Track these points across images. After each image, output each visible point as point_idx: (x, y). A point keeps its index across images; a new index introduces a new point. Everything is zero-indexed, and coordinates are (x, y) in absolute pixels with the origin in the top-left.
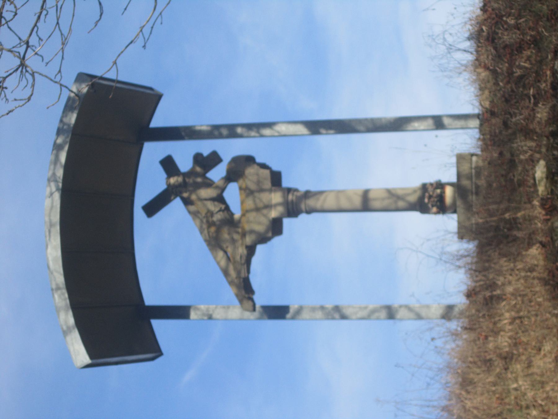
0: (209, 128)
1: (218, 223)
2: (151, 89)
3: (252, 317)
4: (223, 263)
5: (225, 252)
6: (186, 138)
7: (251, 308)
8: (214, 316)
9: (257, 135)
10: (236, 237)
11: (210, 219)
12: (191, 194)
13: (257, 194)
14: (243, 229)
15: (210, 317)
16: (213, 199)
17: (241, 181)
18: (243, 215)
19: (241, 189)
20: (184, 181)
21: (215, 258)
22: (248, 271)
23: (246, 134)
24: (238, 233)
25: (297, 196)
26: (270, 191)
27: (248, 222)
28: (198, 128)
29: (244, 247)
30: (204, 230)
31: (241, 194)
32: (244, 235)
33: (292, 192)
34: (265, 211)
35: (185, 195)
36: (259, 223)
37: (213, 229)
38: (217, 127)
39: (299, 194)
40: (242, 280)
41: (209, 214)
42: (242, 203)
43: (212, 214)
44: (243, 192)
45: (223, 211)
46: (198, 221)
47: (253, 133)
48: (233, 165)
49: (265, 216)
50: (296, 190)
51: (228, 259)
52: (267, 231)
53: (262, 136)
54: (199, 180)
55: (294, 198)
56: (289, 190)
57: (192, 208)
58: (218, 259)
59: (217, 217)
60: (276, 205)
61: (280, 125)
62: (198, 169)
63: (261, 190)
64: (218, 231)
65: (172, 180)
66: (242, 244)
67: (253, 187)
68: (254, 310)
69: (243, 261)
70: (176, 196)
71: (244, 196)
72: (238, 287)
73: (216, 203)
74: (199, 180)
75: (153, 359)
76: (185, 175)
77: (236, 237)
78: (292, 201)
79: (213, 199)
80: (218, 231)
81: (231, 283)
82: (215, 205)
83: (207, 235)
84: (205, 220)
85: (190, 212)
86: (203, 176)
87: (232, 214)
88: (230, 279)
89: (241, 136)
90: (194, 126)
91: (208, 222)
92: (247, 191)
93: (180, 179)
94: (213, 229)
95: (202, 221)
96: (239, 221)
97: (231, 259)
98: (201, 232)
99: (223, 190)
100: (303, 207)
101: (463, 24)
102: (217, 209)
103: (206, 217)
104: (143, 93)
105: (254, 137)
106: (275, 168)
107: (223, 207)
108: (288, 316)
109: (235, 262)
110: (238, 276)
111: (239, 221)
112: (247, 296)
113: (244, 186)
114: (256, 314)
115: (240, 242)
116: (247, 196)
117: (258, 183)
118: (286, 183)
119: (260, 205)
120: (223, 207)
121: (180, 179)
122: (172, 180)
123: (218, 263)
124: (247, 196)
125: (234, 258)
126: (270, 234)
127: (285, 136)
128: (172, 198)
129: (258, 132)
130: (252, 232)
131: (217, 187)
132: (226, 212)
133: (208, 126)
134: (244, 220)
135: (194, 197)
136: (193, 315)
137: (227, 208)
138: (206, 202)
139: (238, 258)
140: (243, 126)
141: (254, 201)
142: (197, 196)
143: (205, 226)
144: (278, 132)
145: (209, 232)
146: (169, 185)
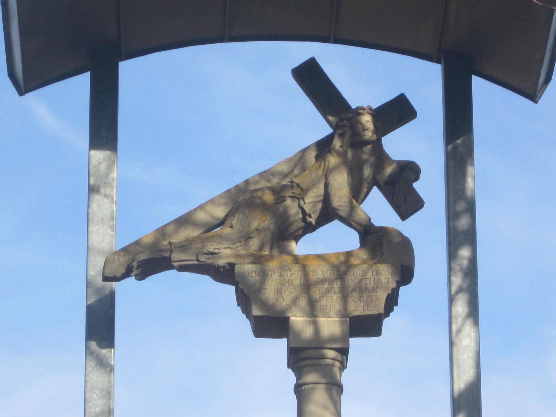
0: (469, 193)
1: (281, 208)
2: (548, 79)
3: (92, 273)
4: (202, 216)
5: (222, 223)
6: (257, 178)
7: (109, 273)
8: (97, 198)
9: (454, 289)
10: (254, 243)
11: (289, 193)
12: (339, 154)
13: (337, 285)
14: (271, 257)
15: (93, 190)
16: (326, 199)
17: (363, 255)
18: (296, 259)
19: (349, 254)
20: (367, 143)
21: (212, 201)
22: (182, 269)
23: (456, 267)
24: (261, 248)
25: (333, 366)
26: (344, 314)
27: (283, 268)
28: (470, 169)
29: (232, 260)
30: (269, 181)
31: (338, 255)
32: (258, 259)
33: (339, 357)
34: (303, 302)
35: (337, 143)
36: (279, 292)
37: (269, 197)
38: (471, 208)
39: (336, 370)
40: (167, 255)
41: (297, 191)
42: (320, 257)
43: (299, 198)
44: (342, 258)
45: (304, 220)
46: (285, 168)
47: (457, 280)
48: (398, 239)
49: (295, 301)
50: (343, 366)
51: (210, 228)
52: (263, 304)
53: (451, 300)
54: (367, 172)
55: (329, 361)
56: (344, 352)
57: (312, 156)
58: (210, 208)
59: (292, 207)
60: (315, 324)
61: (473, 335)
62: (389, 170)
63: (345, 296)
64: (264, 207)
65: (367, 119)
66: (238, 256)
67: (352, 279)
68: (106, 279)
69: (203, 258)
70: (335, 127)
71: (334, 261)
72: (154, 247)
73: (320, 206)
74: (367, 172)
75: (12, 75)
76: (378, 144)
77: (254, 243)
78: (324, 357)
79: (326, 199)
80: (264, 207)
81: (162, 232)
82: (315, 203)
83: (258, 187)
84: (285, 182)
85: (304, 151)
86: (375, 182)
87: (297, 239)
88: (170, 229)
89: (452, 255)
90: (473, 164)
91: (284, 188)
92: (343, 268)
93: (369, 135)
94: (269, 197)
95: (285, 176)
96: (285, 251)
97: (209, 234)
98: (264, 175)
99: (347, 221)
100: (311, 378)
101: (313, 204)
102: (307, 209)
103: (292, 185)
104: (541, 61)
105: (450, 283)
106: (387, 323)
107: (313, 220)
108: (93, 345)
109: (203, 240)
110: (172, 247)
111: (285, 251)
112: (135, 264)
113: (355, 261)
114: (99, 281)
115: (242, 252)
116: (335, 268)
117: (361, 289)
118: (355, 343)
119: (316, 293)
120: (313, 220)
121: (369, 135)
122: (367, 119)
123: (201, 207)
124: (335, 268)
125: (208, 239)
126: (256, 312)
127: (452, 344)
128: (331, 118)
129: (460, 290)
130: (264, 275)
131: (352, 209)
132: (302, 224)
133: (474, 192)
134: (288, 259)
135: (333, 160)
136: (98, 155)
137: (309, 228)
138: (321, 186)
139: (211, 247)
140: (473, 261)
141: (323, 281)
142: (336, 168)
143: (275, 181)
144: (459, 331)
145: (262, 190)
146: (358, 112)
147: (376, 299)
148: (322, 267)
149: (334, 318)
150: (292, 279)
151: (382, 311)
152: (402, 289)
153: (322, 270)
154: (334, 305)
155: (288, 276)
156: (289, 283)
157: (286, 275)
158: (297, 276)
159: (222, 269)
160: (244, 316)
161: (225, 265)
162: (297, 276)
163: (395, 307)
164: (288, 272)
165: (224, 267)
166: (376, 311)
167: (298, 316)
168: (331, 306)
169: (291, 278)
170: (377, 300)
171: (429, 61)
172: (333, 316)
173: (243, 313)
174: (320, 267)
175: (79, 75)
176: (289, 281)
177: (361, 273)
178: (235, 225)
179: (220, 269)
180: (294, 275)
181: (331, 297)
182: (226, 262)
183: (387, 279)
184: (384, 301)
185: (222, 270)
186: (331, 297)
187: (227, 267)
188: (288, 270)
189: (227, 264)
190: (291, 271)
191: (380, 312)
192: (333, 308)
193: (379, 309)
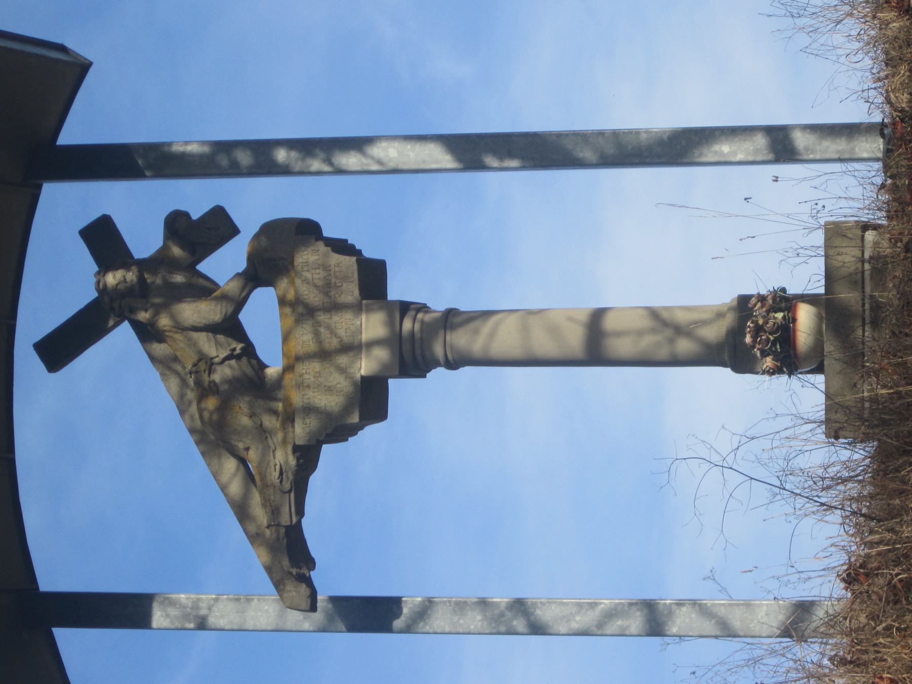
151: (354, 259)
153: (303, 334)
160: (360, 433)
169: (312, 373)
170: (340, 265)
173: (356, 434)
184: (341, 256)
190: (303, 374)
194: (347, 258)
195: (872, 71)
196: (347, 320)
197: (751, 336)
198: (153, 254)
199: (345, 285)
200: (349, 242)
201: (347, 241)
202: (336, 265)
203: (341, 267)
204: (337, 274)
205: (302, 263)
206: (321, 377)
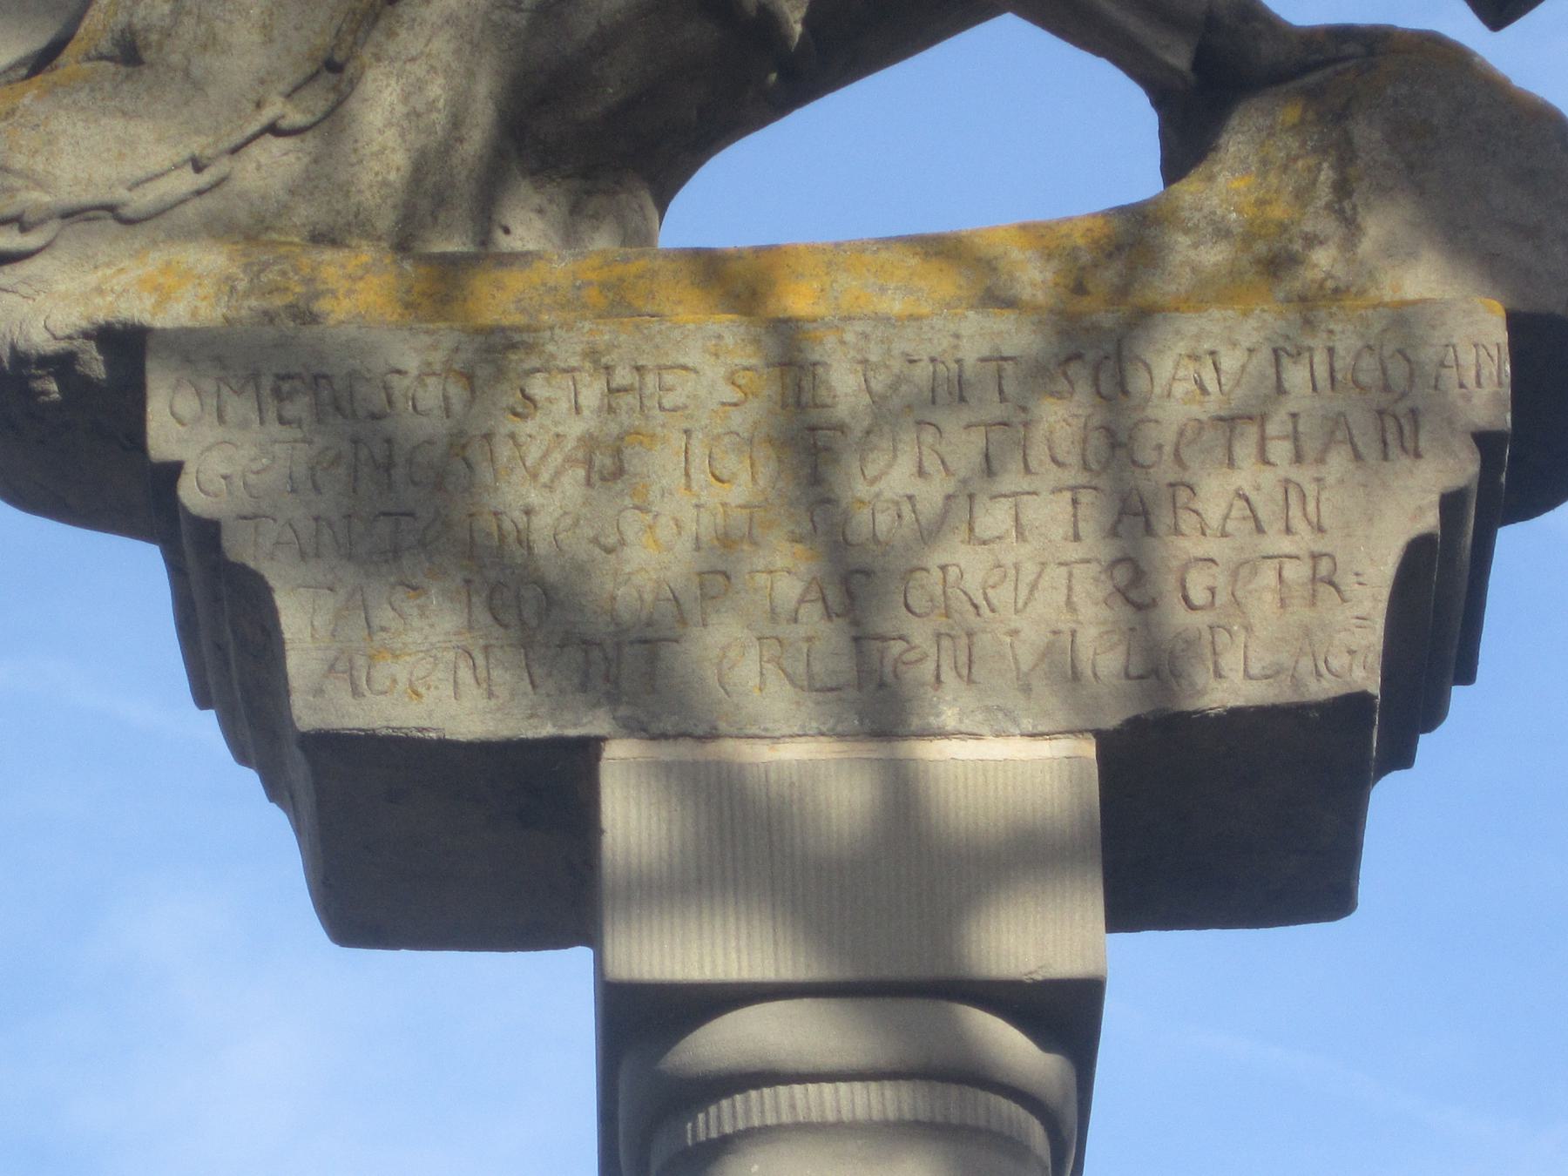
147: (1314, 579)
148: (866, 336)
149: (971, 743)
150: (620, 438)
151: (1366, 677)
152: (1510, 540)
153: (865, 362)
154: (970, 635)
155: (586, 413)
156: (597, 463)
157: (564, 405)
158: (661, 408)
159: (54, 387)
160: (250, 778)
161: (78, 343)
162: (661, 408)
163: (1421, 736)
164: (584, 377)
165: (62, 364)
166: (1319, 674)
167: (669, 728)
168: (946, 643)
169: (614, 428)
170: (1325, 590)
171: (1106, 916)
172: (963, 728)
173: (242, 757)
174: (849, 337)
175: (143, 543)
176: (591, 453)
177: (1181, 373)
178: (154, 37)
179: (37, 385)
180: (629, 399)
181: (943, 568)
182: (85, 324)
183: (1396, 418)
184: (1385, 593)
185: (46, 393)
186: (943, 568)
187: (95, 365)
188: (588, 365)
189: (86, 335)
190: (608, 369)
191: (1356, 689)
192: (963, 659)
193: (1346, 659)
194: (1373, 637)
195: (905, 643)
196: (964, 641)
197: (1332, 167)
198: (1286, 23)
199: (1179, 397)
200: (1458, 693)
201: (1467, 675)
202: (1324, 567)
203: (1313, 601)
204: (1268, 576)
205: (1331, 351)
206: (589, 483)
